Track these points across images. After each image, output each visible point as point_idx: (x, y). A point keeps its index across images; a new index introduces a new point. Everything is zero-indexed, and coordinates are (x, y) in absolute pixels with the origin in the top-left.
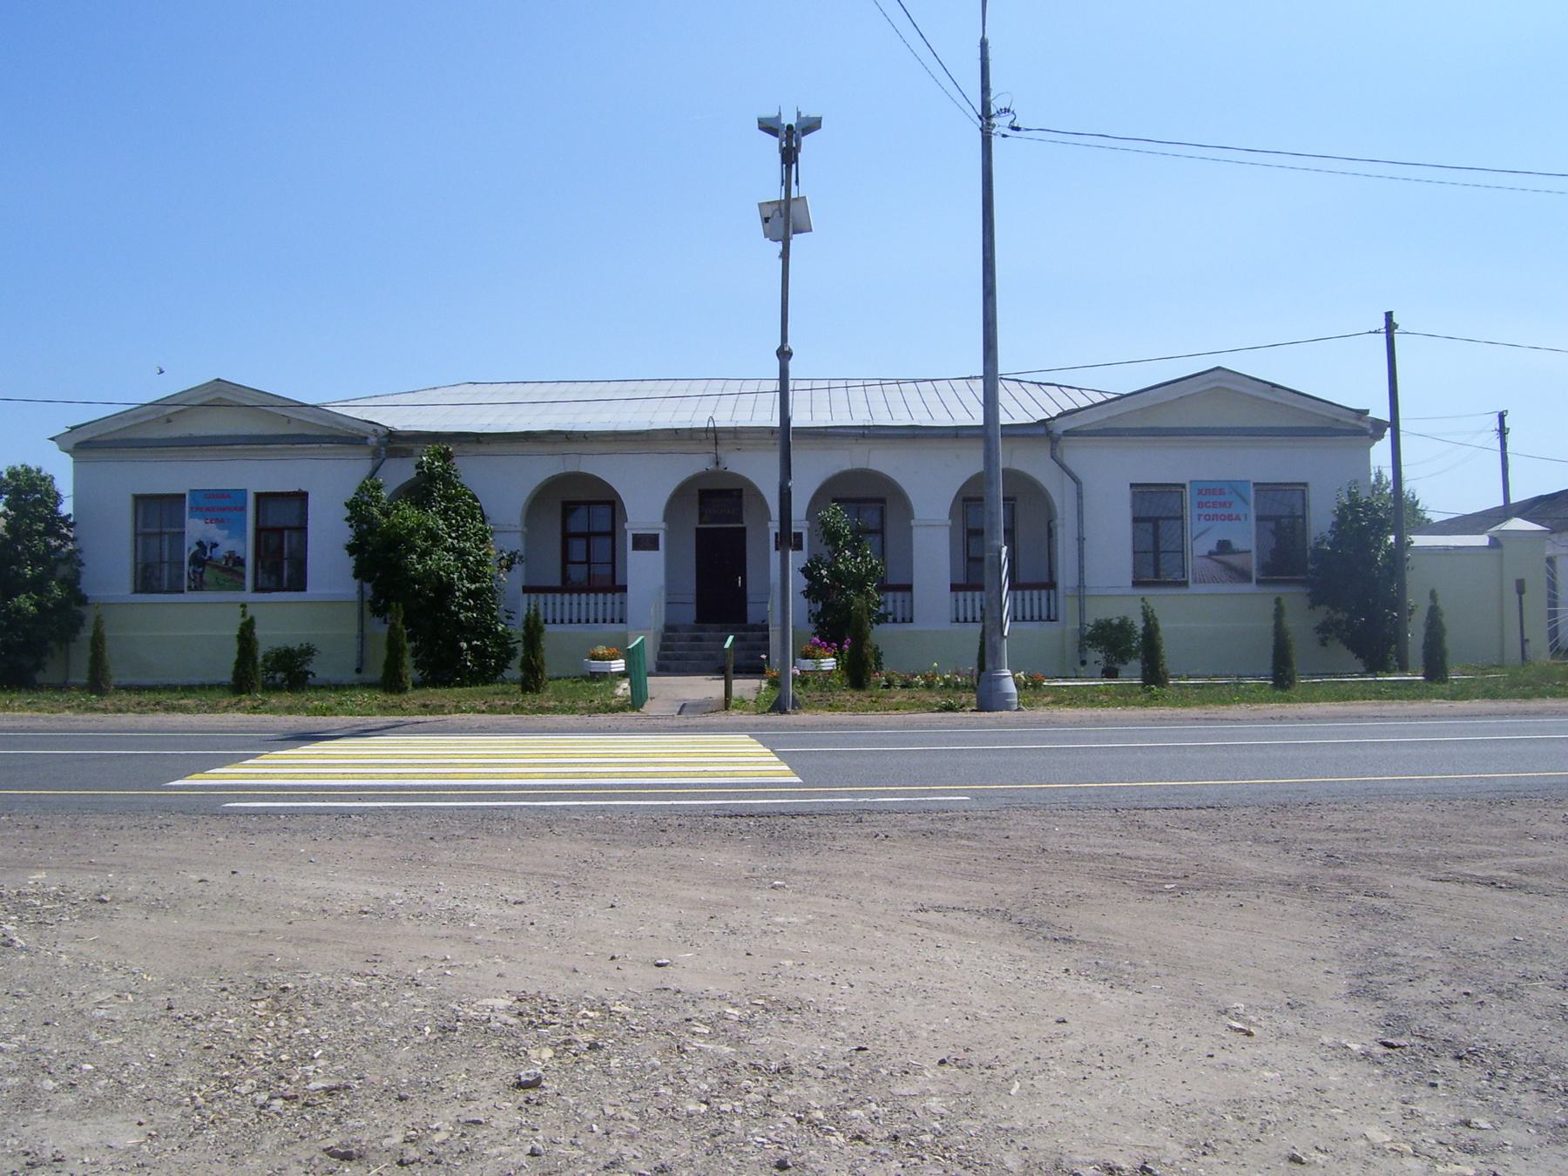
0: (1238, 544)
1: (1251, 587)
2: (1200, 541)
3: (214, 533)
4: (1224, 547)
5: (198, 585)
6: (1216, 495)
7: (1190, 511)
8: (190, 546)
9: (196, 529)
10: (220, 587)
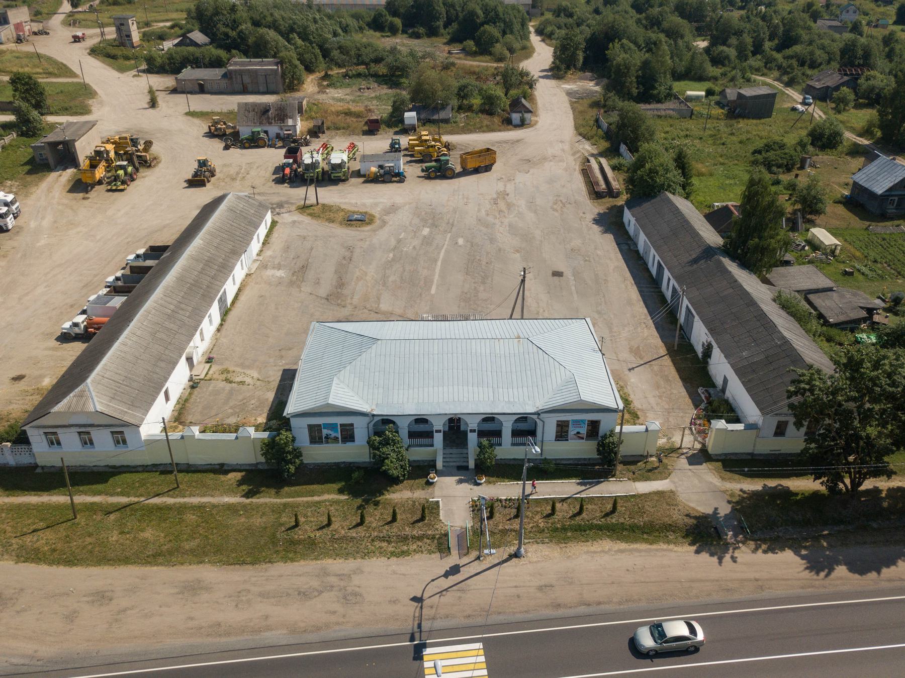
0: (581, 432)
1: (584, 441)
2: (572, 431)
3: (330, 432)
4: (578, 433)
5: (327, 443)
6: (577, 423)
7: (570, 426)
8: (324, 435)
9: (325, 432)
10: (332, 443)
